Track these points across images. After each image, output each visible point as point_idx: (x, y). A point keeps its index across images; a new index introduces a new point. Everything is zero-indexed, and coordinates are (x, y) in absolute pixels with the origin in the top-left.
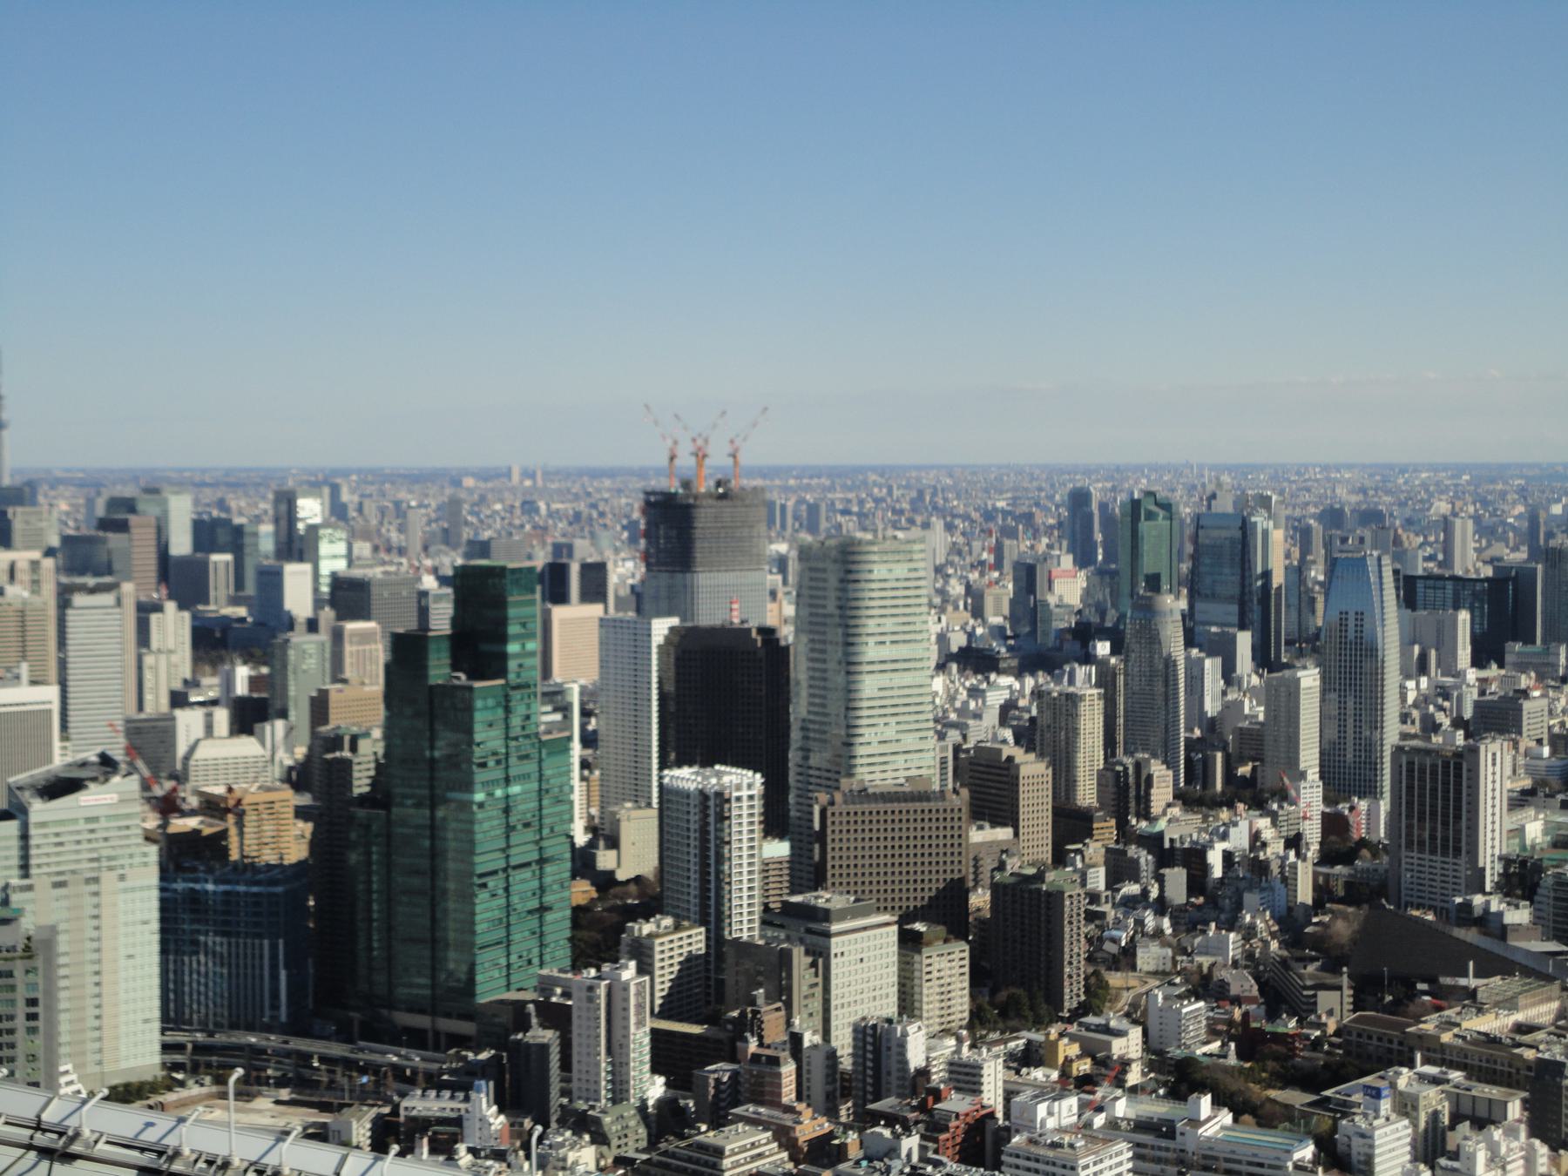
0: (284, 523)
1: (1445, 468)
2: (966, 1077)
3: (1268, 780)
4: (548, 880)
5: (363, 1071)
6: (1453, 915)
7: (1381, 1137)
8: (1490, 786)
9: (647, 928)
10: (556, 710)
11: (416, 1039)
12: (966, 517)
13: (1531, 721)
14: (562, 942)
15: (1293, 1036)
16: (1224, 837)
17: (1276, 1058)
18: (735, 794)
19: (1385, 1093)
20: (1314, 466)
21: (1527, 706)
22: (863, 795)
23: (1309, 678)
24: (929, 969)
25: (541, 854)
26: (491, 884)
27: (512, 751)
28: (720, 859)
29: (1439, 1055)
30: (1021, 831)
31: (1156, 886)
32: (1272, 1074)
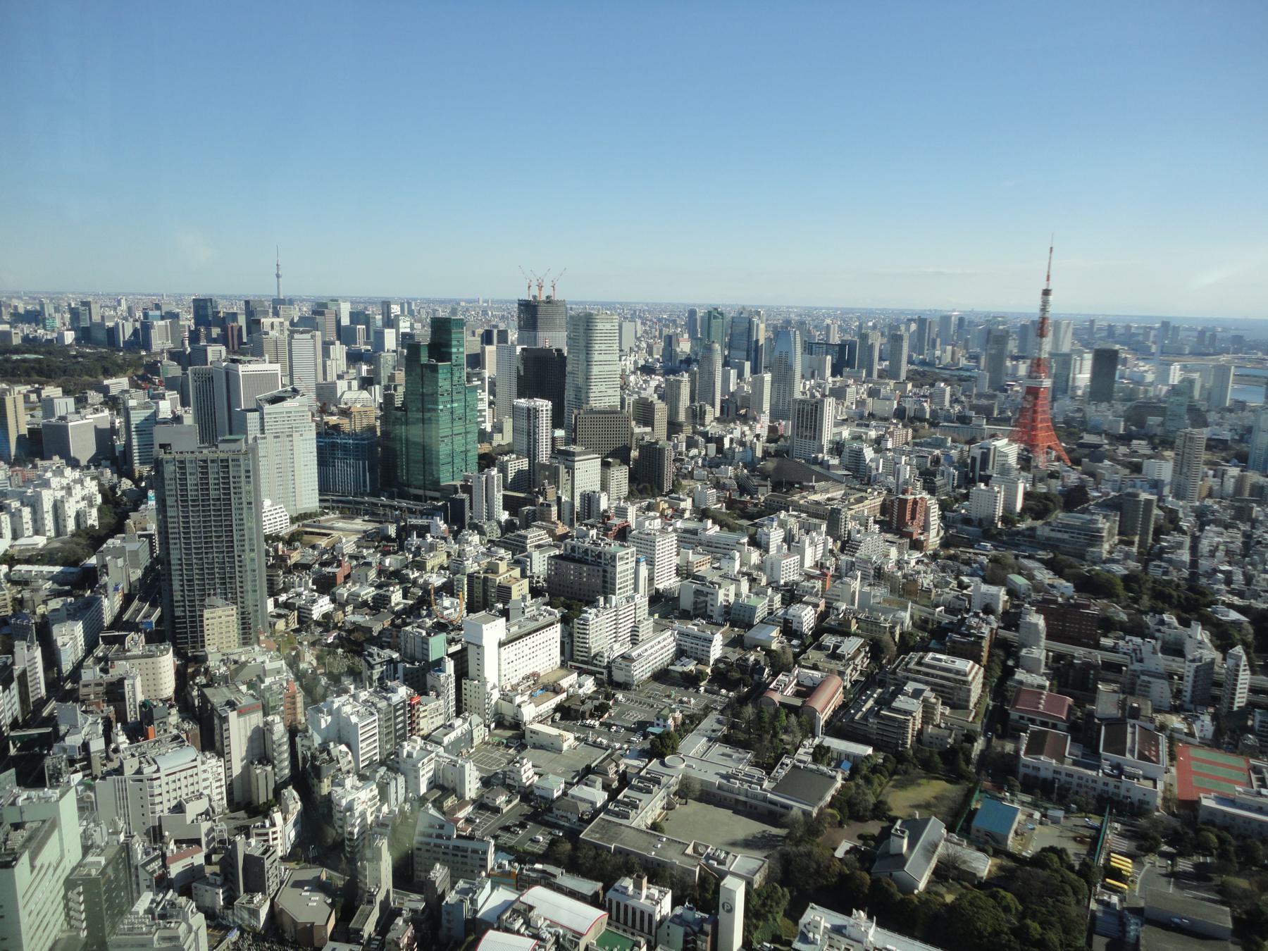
1: (832, 309)
2: (622, 512)
7: (455, 333)
9: (506, 458)
11: (417, 498)
12: (651, 321)
16: (732, 433)
21: (848, 390)
22: (592, 411)
23: (768, 377)
28: (535, 433)
29: (799, 508)
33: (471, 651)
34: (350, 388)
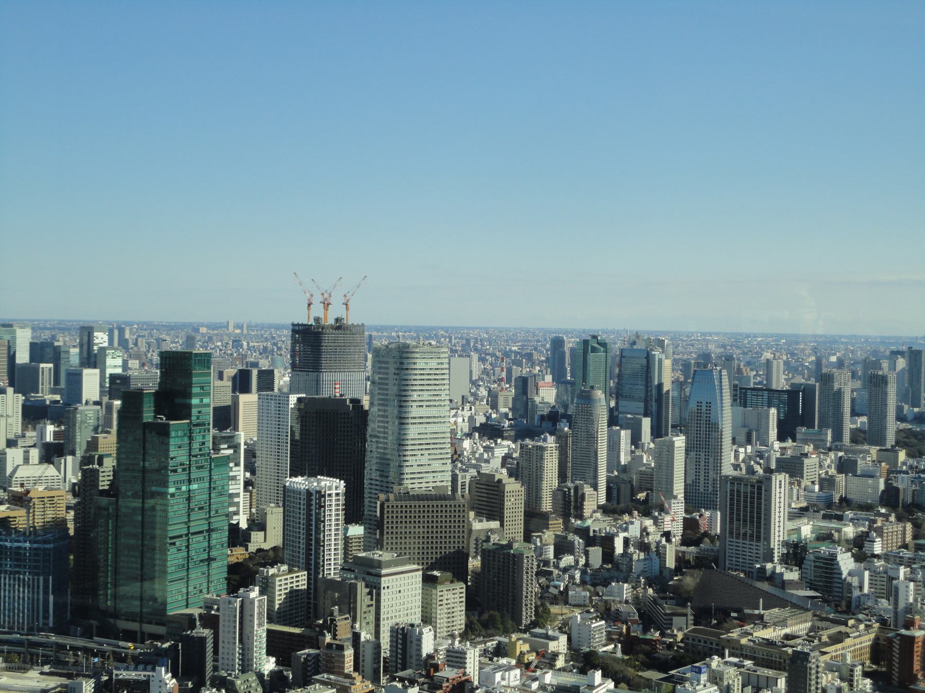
0: (85, 347)
1: (772, 336)
2: (456, 659)
3: (655, 498)
4: (213, 542)
5: (95, 655)
6: (755, 575)
8: (778, 500)
9: (272, 571)
10: (229, 448)
11: (130, 636)
12: (493, 355)
13: (809, 471)
14: (221, 580)
15: (655, 641)
16: (626, 530)
18: (328, 492)
19: (703, 670)
20: (697, 333)
22: (407, 496)
23: (680, 442)
24: (441, 598)
25: (209, 526)
26: (177, 543)
27: (193, 463)
29: (739, 651)
30: (505, 524)
31: (584, 557)
32: (643, 663)
34: (26, 460)
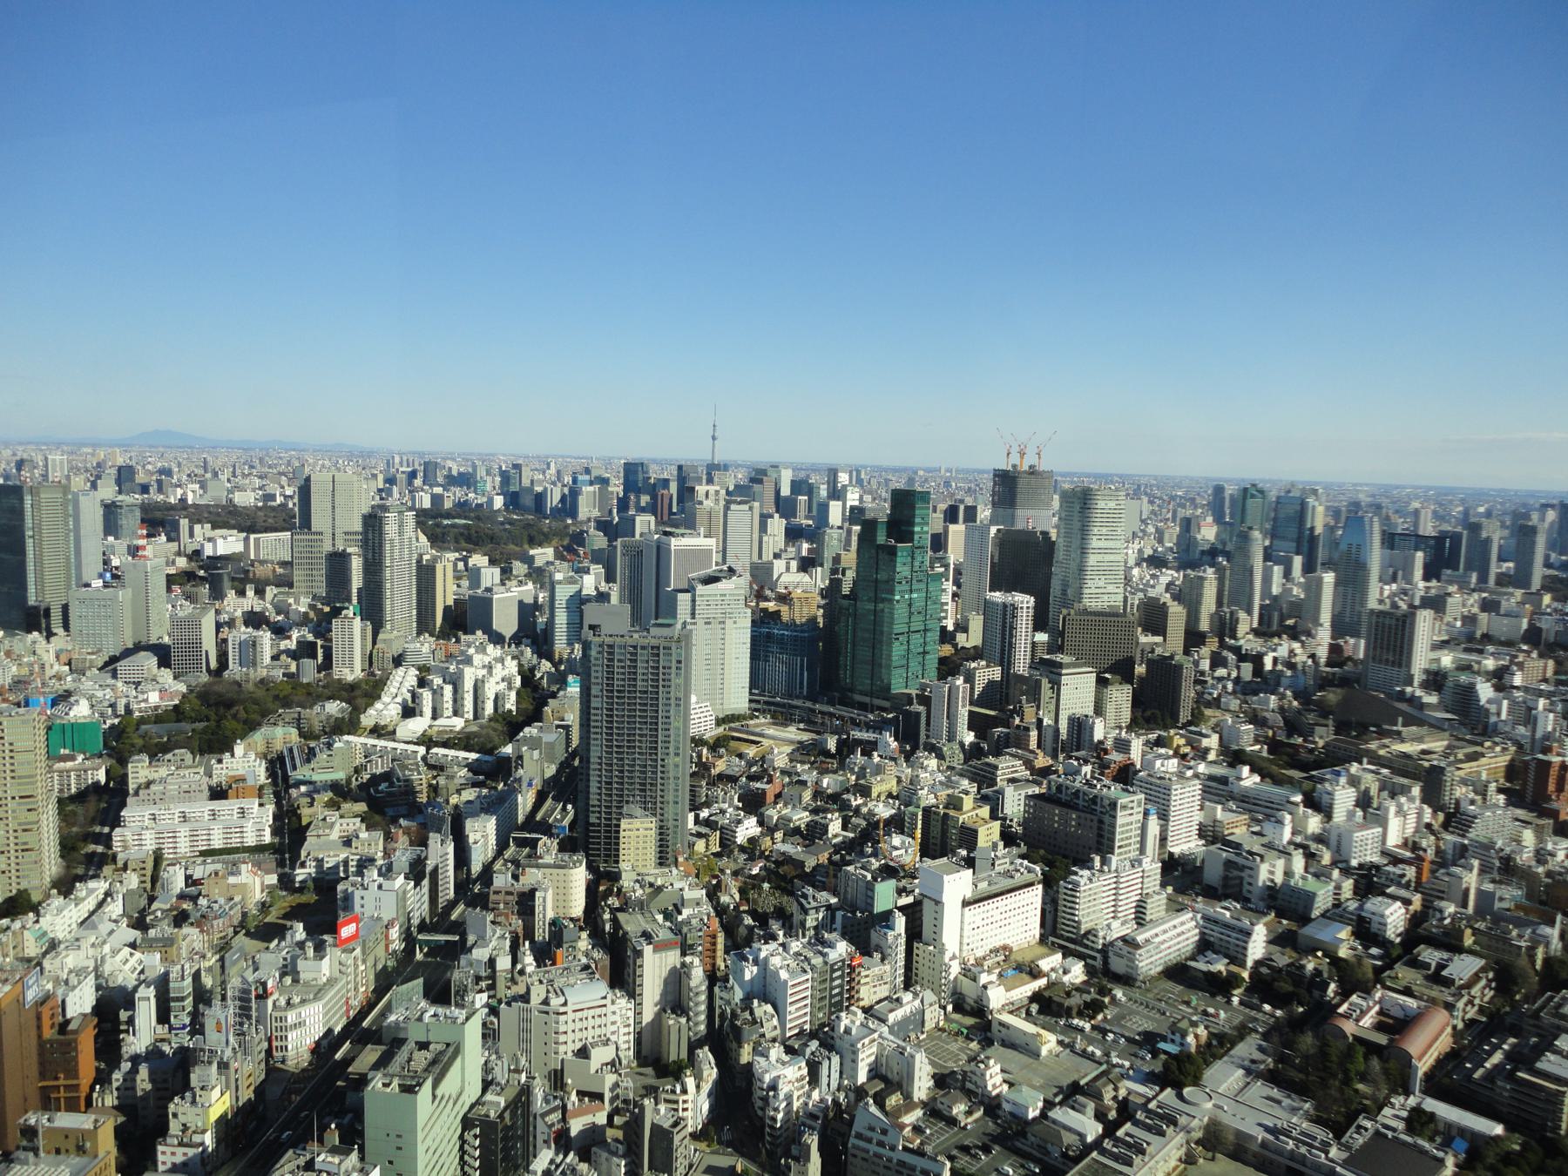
2: (1123, 746)
4: (928, 639)
9: (973, 665)
16: (1274, 650)
17: (1288, 755)
21: (1450, 600)
22: (1085, 612)
23: (1329, 578)
28: (1011, 636)
29: (1376, 760)
33: (928, 907)
34: (788, 569)
